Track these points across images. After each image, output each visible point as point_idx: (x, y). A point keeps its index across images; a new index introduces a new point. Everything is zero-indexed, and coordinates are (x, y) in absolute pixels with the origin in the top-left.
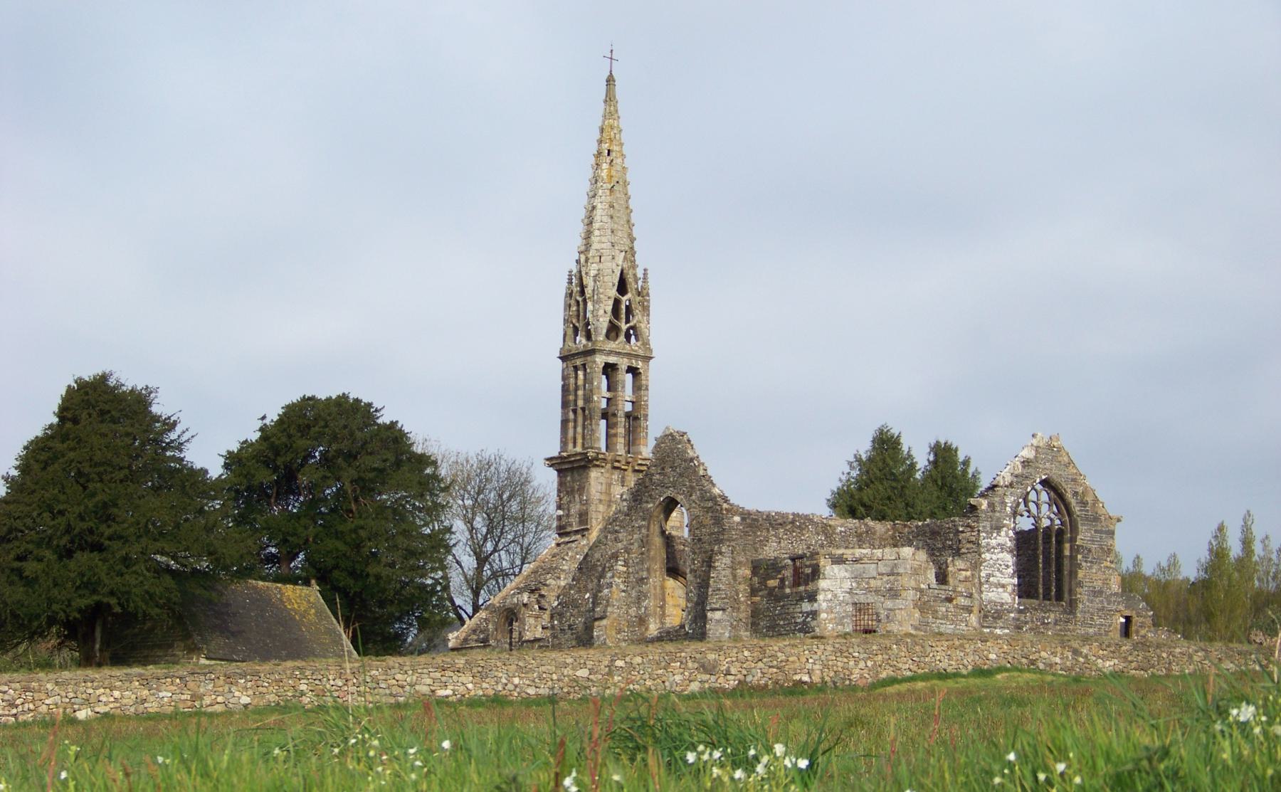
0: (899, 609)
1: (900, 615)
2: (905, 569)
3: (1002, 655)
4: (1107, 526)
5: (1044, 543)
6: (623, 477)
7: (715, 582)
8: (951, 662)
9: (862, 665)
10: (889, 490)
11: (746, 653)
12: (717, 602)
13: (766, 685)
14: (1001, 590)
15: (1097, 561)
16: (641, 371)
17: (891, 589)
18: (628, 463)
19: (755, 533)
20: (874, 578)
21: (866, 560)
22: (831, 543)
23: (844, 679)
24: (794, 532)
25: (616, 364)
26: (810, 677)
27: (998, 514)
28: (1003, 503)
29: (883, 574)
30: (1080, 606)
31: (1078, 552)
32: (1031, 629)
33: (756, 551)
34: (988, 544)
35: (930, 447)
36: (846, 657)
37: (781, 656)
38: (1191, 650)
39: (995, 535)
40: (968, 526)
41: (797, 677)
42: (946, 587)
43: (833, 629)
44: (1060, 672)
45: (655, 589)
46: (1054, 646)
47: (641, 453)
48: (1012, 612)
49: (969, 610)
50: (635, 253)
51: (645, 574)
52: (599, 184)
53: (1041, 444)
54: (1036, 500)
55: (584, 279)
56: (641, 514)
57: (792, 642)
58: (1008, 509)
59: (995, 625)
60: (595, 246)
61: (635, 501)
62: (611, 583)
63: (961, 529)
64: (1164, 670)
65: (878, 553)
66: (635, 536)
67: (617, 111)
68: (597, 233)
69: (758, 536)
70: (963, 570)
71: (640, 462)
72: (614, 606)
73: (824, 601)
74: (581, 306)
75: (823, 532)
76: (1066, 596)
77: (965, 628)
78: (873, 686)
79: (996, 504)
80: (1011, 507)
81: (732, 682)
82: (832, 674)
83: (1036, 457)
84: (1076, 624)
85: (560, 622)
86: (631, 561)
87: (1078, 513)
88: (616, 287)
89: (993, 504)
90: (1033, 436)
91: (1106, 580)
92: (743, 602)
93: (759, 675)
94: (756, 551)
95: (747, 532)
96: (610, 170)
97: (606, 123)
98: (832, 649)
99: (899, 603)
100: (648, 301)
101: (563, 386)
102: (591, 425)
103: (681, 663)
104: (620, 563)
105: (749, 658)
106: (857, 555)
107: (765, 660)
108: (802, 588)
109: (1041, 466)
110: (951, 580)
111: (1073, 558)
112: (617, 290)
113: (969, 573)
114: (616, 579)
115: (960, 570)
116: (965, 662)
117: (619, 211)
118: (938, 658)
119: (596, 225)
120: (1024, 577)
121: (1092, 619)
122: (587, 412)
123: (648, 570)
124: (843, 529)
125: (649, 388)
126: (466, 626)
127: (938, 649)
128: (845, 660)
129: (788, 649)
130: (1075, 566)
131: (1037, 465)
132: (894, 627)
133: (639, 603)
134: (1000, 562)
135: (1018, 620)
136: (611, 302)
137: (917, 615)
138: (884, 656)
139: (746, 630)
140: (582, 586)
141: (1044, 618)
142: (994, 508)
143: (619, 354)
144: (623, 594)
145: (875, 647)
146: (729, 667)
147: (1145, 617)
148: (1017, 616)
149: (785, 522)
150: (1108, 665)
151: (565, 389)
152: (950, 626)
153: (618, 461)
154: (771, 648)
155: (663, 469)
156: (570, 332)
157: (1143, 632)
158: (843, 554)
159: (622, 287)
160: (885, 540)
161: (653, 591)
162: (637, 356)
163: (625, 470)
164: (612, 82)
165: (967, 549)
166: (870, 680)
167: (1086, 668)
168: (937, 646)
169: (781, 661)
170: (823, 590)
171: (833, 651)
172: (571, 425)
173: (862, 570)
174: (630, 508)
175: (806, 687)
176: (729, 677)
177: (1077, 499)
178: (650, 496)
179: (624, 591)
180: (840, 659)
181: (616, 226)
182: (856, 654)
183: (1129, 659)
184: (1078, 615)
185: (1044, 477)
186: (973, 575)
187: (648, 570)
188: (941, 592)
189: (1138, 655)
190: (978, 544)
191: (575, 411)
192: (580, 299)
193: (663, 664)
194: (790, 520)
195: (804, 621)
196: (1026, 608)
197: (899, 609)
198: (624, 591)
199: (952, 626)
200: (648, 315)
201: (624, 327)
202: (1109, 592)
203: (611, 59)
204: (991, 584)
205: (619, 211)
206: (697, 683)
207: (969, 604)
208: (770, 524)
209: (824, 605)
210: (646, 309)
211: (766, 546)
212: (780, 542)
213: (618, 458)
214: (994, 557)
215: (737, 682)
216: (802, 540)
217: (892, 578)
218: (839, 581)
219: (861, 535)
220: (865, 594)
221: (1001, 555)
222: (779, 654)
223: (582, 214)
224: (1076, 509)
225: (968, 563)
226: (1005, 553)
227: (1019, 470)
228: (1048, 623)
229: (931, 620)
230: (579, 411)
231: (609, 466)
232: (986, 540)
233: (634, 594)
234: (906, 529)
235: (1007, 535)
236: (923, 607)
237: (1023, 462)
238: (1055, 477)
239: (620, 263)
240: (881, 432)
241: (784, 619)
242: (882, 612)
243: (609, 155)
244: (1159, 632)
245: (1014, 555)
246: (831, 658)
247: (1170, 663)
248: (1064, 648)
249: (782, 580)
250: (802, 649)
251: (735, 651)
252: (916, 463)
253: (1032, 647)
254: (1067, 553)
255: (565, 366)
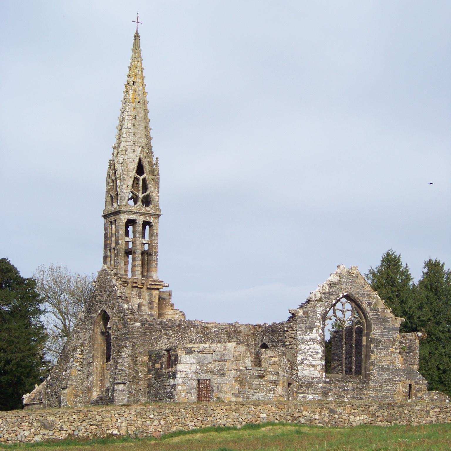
0: (225, 383)
1: (226, 387)
2: (229, 357)
3: (271, 414)
4: (394, 325)
5: (342, 339)
6: (140, 293)
7: (120, 365)
8: (228, 420)
9: (156, 423)
10: (390, 293)
11: (74, 416)
12: (121, 379)
13: (88, 437)
14: (312, 369)
15: (386, 348)
16: (153, 224)
17: (220, 370)
18: (143, 284)
19: (151, 333)
20: (211, 363)
21: (206, 352)
22: (208, 339)
23: (142, 433)
24: (180, 332)
25: (135, 220)
26: (119, 432)
27: (310, 319)
28: (315, 312)
29: (216, 361)
30: (372, 378)
31: (371, 342)
32: (335, 394)
33: (152, 345)
34: (303, 339)
35: (425, 263)
36: (145, 418)
37: (99, 418)
38: (428, 408)
39: (308, 333)
40: (290, 327)
41: (109, 432)
42: (260, 369)
43: (185, 396)
44: (319, 425)
45: (97, 369)
46: (314, 407)
47: (152, 277)
48: (320, 383)
49: (276, 383)
50: (152, 147)
51: (91, 360)
52: (127, 104)
53: (343, 272)
54: (342, 309)
55: (116, 165)
56: (90, 321)
57: (108, 408)
58: (318, 315)
59: (307, 392)
60: (123, 144)
61: (88, 312)
62: (72, 365)
63: (286, 329)
64: (405, 421)
65: (214, 346)
66: (87, 335)
67: (140, 56)
68: (124, 135)
69: (153, 335)
70: (272, 357)
71: (150, 283)
72: (73, 380)
73: (180, 378)
74: (115, 183)
75: (202, 331)
76: (363, 371)
77: (273, 395)
78: (165, 437)
79: (310, 312)
80: (320, 314)
81: (64, 435)
82: (134, 429)
83: (339, 281)
84: (369, 390)
85: (51, 390)
86: (85, 351)
87: (371, 317)
88: (135, 170)
89: (307, 312)
90: (338, 267)
91: (392, 360)
92: (142, 378)
93: (83, 430)
94: (152, 345)
95: (145, 333)
96: (133, 94)
97: (133, 64)
98: (134, 413)
99: (225, 379)
100: (158, 179)
101: (105, 234)
102: (118, 259)
103: (29, 423)
104: (78, 352)
105: (76, 419)
106: (201, 348)
107: (87, 420)
108: (170, 369)
109: (343, 286)
110: (263, 364)
111: (368, 346)
112: (136, 172)
113: (276, 359)
114: (74, 363)
115: (270, 357)
116: (240, 420)
117: (140, 121)
118: (218, 417)
119: (124, 130)
120: (348, 359)
121: (381, 386)
122: (116, 251)
123: (93, 357)
124: (216, 329)
125: (159, 235)
126: (35, 390)
127: (218, 411)
128: (144, 420)
129: (104, 413)
130: (370, 352)
131: (340, 286)
132: (222, 395)
133: (88, 378)
134: (311, 350)
135: (325, 388)
136: (131, 180)
137: (237, 387)
138: (175, 417)
139: (144, 396)
140: (61, 367)
141: (344, 386)
142: (308, 315)
143: (137, 213)
144: (80, 373)
145: (167, 411)
146: (62, 425)
147: (421, 385)
148: (324, 385)
149: (173, 326)
150: (358, 420)
151: (106, 237)
152: (261, 394)
153: (136, 283)
154: (91, 413)
155: (101, 292)
156: (109, 199)
157: (419, 394)
158: (192, 348)
159: (140, 170)
160: (247, 336)
161: (95, 371)
162: (150, 215)
163: (142, 288)
164: (137, 38)
165: (290, 342)
166: (162, 433)
167: (340, 421)
168: (217, 409)
169: (99, 421)
170: (180, 371)
171: (134, 414)
172: (108, 259)
173: (203, 358)
174: (85, 317)
175: (115, 438)
176: (62, 432)
177: (370, 307)
178: (95, 309)
179: (80, 371)
180: (140, 419)
181: (136, 130)
182: (152, 416)
183: (377, 415)
184: (371, 384)
185: (345, 294)
186: (279, 360)
187: (93, 357)
188: (255, 371)
189: (384, 412)
190: (296, 339)
191: (110, 250)
192: (114, 178)
193: (16, 424)
194: (177, 324)
195: (170, 391)
196: (331, 380)
197: (225, 383)
198: (80, 371)
199: (264, 394)
200: (158, 188)
201: (141, 196)
202: (394, 369)
203: (137, 22)
204: (305, 365)
205: (140, 121)
206: (39, 436)
207: (277, 379)
208: (162, 327)
209: (180, 381)
210: (157, 184)
211: (159, 341)
212: (169, 339)
213: (135, 281)
214: (307, 347)
215: (67, 435)
216: (186, 337)
217: (221, 363)
218: (189, 365)
219: (230, 333)
220: (205, 373)
221: (313, 346)
222: (97, 417)
223: (117, 123)
224: (370, 314)
225: (276, 353)
226: (316, 344)
227: (327, 289)
228: (347, 390)
229: (247, 390)
230: (113, 250)
231: (130, 286)
232: (301, 336)
233: (86, 373)
234: (261, 329)
235: (317, 333)
236: (241, 381)
237: (330, 284)
238: (353, 294)
239: (138, 154)
240: (388, 254)
241: (161, 390)
242: (215, 385)
243: (133, 85)
244: (432, 394)
245: (323, 346)
246: (133, 418)
247: (410, 417)
248: (323, 408)
249: (162, 364)
250: (114, 413)
251: (66, 415)
252: (410, 274)
253: (296, 409)
254: (364, 343)
255: (106, 221)
